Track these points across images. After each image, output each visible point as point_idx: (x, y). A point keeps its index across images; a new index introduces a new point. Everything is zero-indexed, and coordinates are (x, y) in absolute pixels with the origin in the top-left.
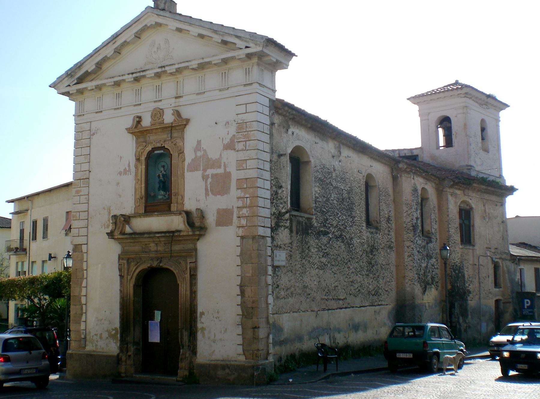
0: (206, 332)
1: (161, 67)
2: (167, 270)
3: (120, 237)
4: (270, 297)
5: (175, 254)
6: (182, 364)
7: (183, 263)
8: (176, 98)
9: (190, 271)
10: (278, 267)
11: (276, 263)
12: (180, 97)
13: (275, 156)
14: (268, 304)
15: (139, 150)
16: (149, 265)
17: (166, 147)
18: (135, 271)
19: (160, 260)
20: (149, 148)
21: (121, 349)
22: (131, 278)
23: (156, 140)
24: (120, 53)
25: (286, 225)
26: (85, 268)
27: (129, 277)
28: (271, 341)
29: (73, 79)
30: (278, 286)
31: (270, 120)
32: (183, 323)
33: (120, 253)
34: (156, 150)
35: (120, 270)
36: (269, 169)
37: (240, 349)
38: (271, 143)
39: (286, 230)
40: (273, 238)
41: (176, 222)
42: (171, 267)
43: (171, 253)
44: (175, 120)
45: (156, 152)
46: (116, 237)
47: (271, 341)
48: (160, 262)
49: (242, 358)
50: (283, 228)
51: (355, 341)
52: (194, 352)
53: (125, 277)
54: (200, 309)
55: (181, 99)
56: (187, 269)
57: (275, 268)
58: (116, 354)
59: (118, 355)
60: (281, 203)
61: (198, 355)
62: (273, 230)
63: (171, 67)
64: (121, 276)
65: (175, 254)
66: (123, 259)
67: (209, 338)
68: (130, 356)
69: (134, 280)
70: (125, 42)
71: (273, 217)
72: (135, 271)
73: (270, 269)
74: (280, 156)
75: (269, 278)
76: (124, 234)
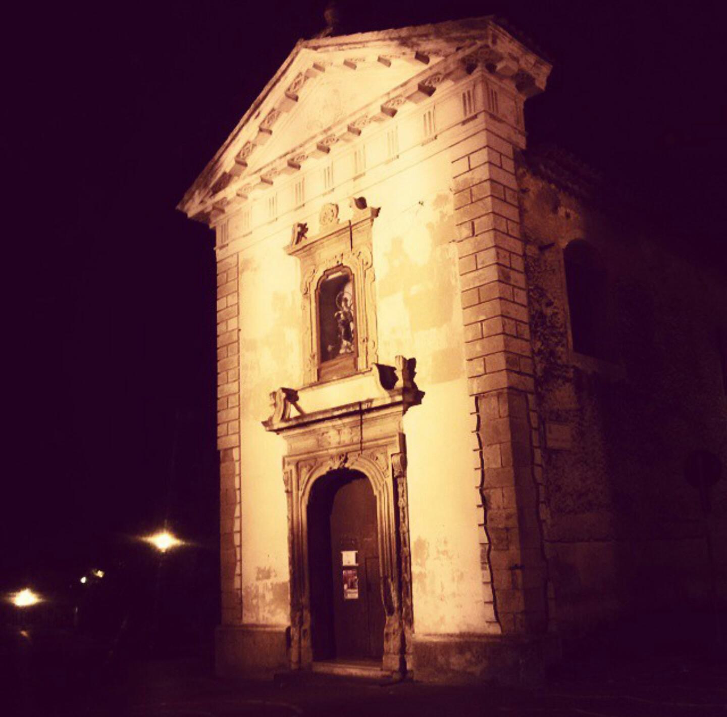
0: (427, 581)
1: (325, 131)
2: (360, 476)
3: (284, 425)
4: (542, 507)
5: (367, 444)
6: (392, 644)
7: (381, 457)
8: (355, 179)
9: (393, 470)
10: (557, 451)
11: (550, 444)
12: (361, 176)
13: (532, 250)
14: (541, 522)
15: (306, 279)
16: (327, 469)
17: (344, 264)
18: (307, 482)
19: (345, 457)
20: (320, 274)
21: (292, 619)
22: (304, 494)
23: (327, 257)
24: (271, 132)
25: (568, 375)
26: (237, 486)
27: (300, 493)
28: (551, 594)
29: (207, 190)
30: (559, 488)
31: (519, 185)
32: (393, 570)
33: (285, 453)
34: (332, 273)
35: (286, 482)
36: (521, 268)
37: (490, 611)
38: (521, 223)
39: (568, 384)
40: (540, 398)
41: (367, 388)
42: (362, 467)
43: (361, 443)
44: (355, 216)
45: (331, 277)
46: (276, 427)
47: (551, 594)
48: (346, 461)
49: (166, 521)
50: (560, 381)
51: (454, 250)
52: (408, 619)
53: (295, 492)
54: (414, 537)
55: (362, 179)
56: (388, 467)
57: (550, 453)
58: (284, 629)
59: (288, 629)
60: (553, 335)
61: (416, 624)
62: (538, 383)
63: (339, 127)
64: (289, 493)
65: (367, 444)
66: (289, 464)
67: (433, 592)
68: (305, 631)
69: (306, 497)
70: (273, 110)
71: (537, 359)
72: (307, 482)
73: (538, 453)
74: (543, 248)
75: (538, 471)
76: (289, 420)
